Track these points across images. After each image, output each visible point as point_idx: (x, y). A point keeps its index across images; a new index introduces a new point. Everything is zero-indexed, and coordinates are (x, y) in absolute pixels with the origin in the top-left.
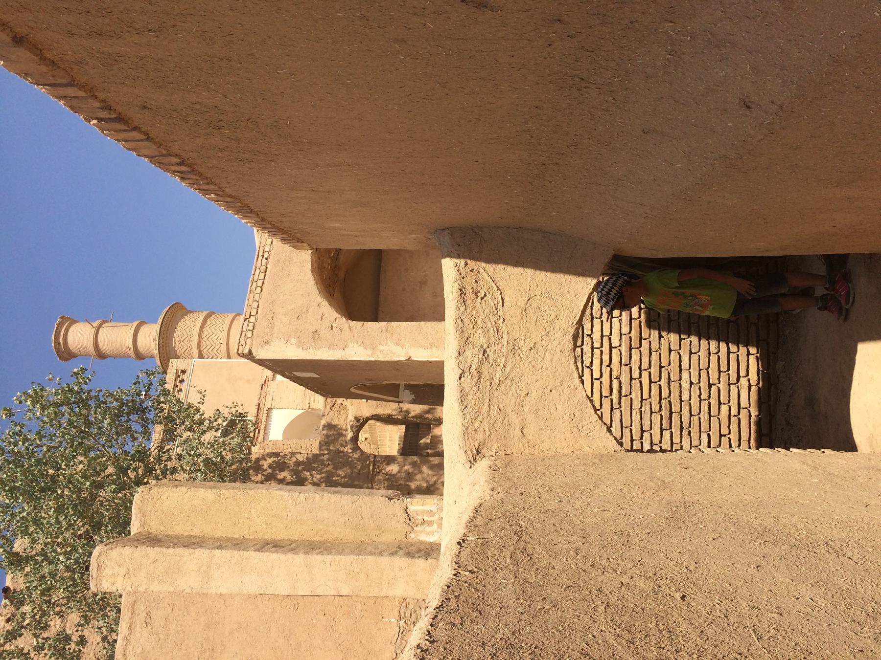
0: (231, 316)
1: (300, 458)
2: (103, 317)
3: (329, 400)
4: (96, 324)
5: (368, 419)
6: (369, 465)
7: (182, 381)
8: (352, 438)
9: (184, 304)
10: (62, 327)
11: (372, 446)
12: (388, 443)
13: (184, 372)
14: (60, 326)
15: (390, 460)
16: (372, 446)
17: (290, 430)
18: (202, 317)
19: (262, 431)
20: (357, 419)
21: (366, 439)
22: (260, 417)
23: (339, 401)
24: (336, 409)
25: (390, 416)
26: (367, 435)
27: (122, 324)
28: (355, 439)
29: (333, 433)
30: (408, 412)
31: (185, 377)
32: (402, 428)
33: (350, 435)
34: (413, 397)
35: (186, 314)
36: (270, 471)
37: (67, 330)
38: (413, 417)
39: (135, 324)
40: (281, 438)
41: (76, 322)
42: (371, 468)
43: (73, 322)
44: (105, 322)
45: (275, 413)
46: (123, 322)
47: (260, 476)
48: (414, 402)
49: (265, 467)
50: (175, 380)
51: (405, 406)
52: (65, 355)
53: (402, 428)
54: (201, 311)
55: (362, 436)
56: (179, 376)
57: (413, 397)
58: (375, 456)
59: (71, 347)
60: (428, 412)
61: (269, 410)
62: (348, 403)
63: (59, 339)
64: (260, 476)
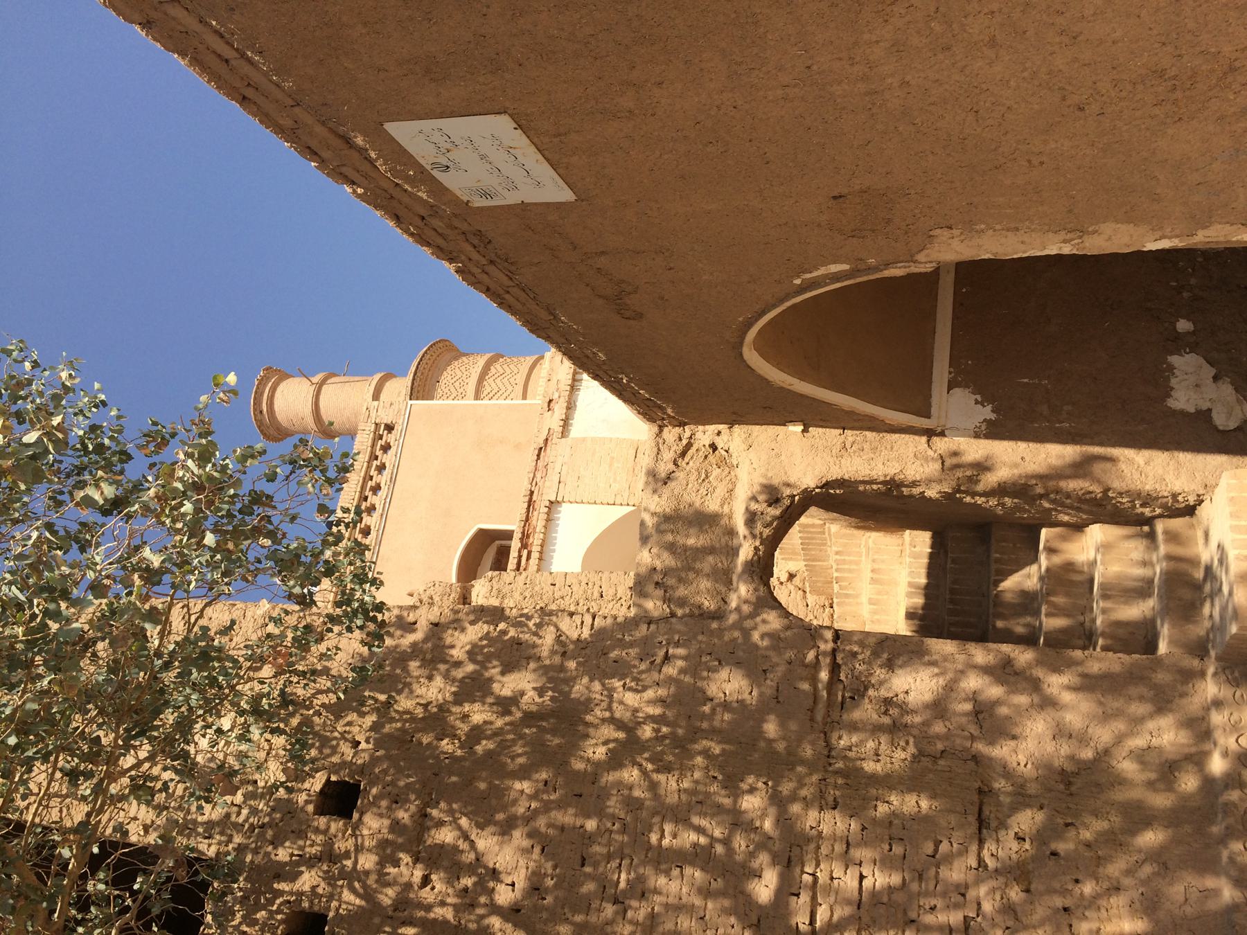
0: (530, 360)
1: (572, 629)
2: (329, 365)
3: (670, 433)
4: (317, 379)
5: (809, 500)
6: (816, 665)
7: (386, 448)
8: (749, 565)
9: (455, 343)
10: (265, 386)
11: (811, 599)
12: (865, 591)
13: (390, 428)
14: (263, 382)
15: (891, 651)
16: (811, 599)
17: (597, 553)
18: (481, 361)
19: (535, 555)
20: (772, 494)
21: (791, 576)
22: (533, 521)
23: (705, 434)
24: (693, 463)
25: (893, 486)
26: (793, 566)
27: (357, 378)
28: (762, 568)
29: (686, 537)
30: (982, 467)
31: (390, 438)
32: (919, 542)
33: (746, 552)
34: (987, 412)
35: (456, 358)
36: (470, 668)
37: (273, 389)
38: (1001, 490)
39: (377, 377)
40: (578, 569)
41: (287, 376)
42: (824, 675)
43: (284, 376)
44: (334, 375)
45: (566, 513)
46: (362, 375)
47: (439, 681)
48: (993, 431)
49: (457, 653)
50: (373, 446)
51: (975, 449)
52: (272, 432)
53: (919, 542)
54: (480, 352)
55: (782, 566)
56: (381, 437)
57: (987, 412)
58: (837, 635)
59: (279, 418)
60: (1080, 468)
61: (553, 505)
62: (734, 439)
63: (260, 404)
64: (439, 681)
